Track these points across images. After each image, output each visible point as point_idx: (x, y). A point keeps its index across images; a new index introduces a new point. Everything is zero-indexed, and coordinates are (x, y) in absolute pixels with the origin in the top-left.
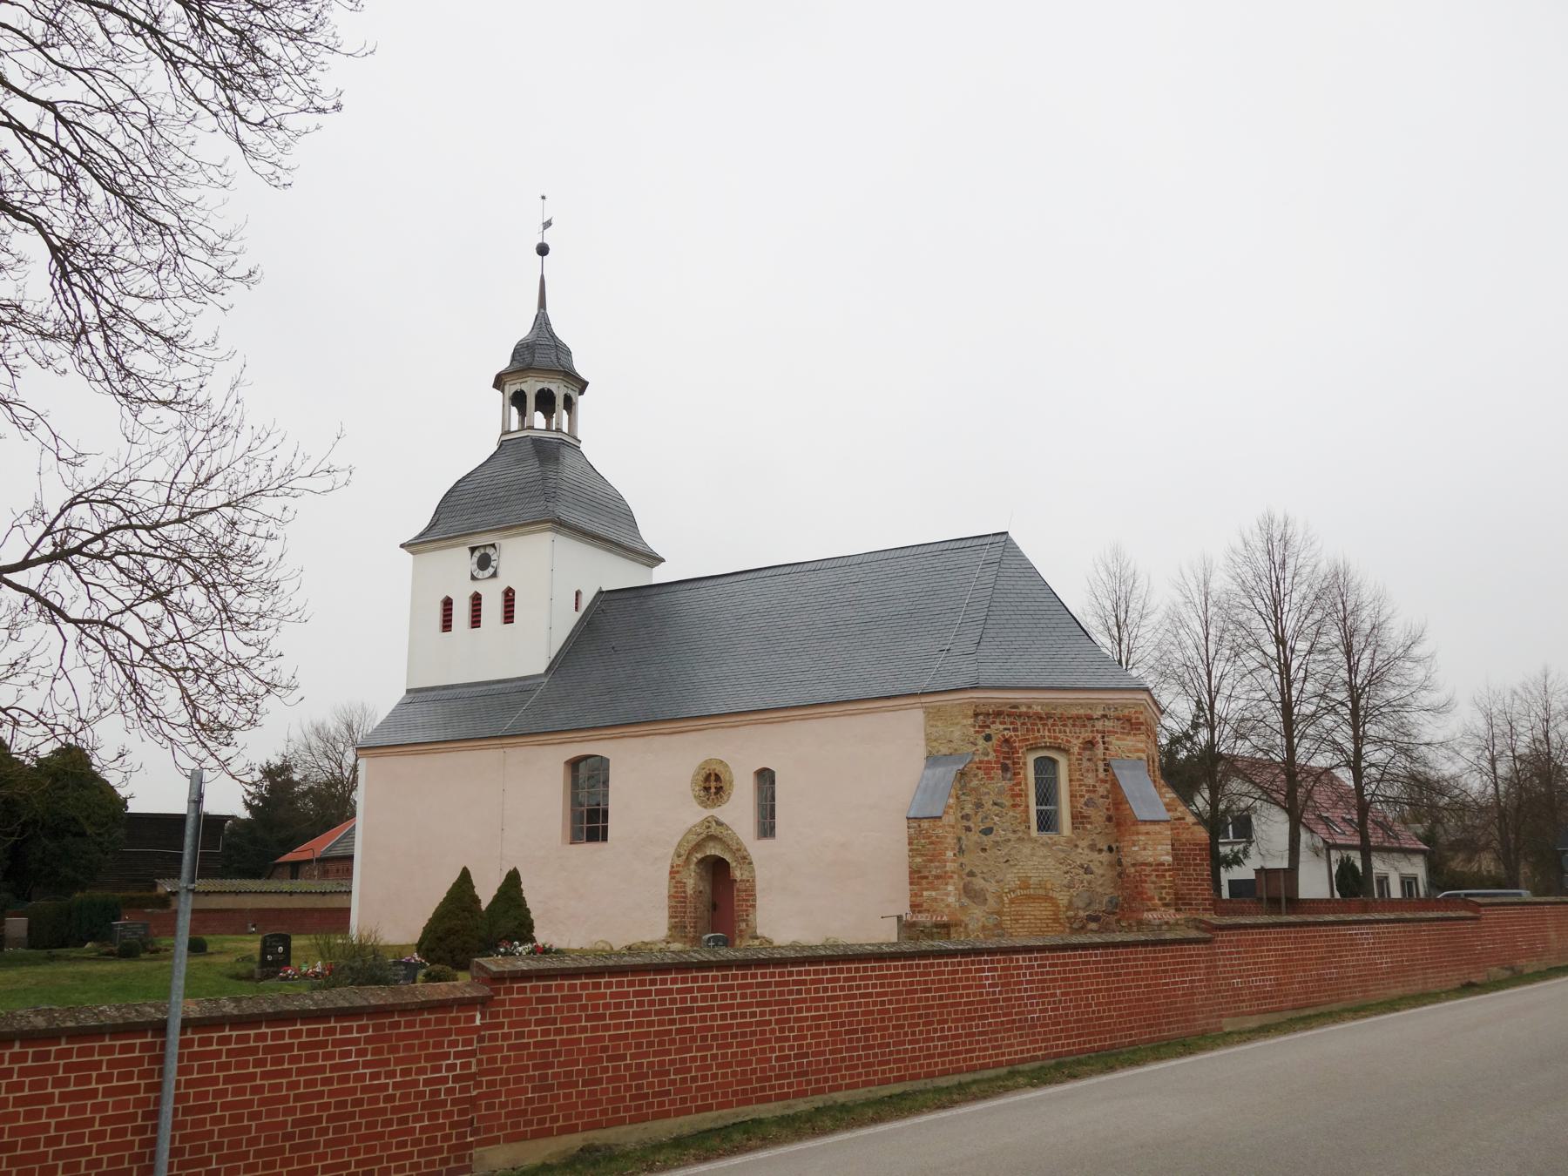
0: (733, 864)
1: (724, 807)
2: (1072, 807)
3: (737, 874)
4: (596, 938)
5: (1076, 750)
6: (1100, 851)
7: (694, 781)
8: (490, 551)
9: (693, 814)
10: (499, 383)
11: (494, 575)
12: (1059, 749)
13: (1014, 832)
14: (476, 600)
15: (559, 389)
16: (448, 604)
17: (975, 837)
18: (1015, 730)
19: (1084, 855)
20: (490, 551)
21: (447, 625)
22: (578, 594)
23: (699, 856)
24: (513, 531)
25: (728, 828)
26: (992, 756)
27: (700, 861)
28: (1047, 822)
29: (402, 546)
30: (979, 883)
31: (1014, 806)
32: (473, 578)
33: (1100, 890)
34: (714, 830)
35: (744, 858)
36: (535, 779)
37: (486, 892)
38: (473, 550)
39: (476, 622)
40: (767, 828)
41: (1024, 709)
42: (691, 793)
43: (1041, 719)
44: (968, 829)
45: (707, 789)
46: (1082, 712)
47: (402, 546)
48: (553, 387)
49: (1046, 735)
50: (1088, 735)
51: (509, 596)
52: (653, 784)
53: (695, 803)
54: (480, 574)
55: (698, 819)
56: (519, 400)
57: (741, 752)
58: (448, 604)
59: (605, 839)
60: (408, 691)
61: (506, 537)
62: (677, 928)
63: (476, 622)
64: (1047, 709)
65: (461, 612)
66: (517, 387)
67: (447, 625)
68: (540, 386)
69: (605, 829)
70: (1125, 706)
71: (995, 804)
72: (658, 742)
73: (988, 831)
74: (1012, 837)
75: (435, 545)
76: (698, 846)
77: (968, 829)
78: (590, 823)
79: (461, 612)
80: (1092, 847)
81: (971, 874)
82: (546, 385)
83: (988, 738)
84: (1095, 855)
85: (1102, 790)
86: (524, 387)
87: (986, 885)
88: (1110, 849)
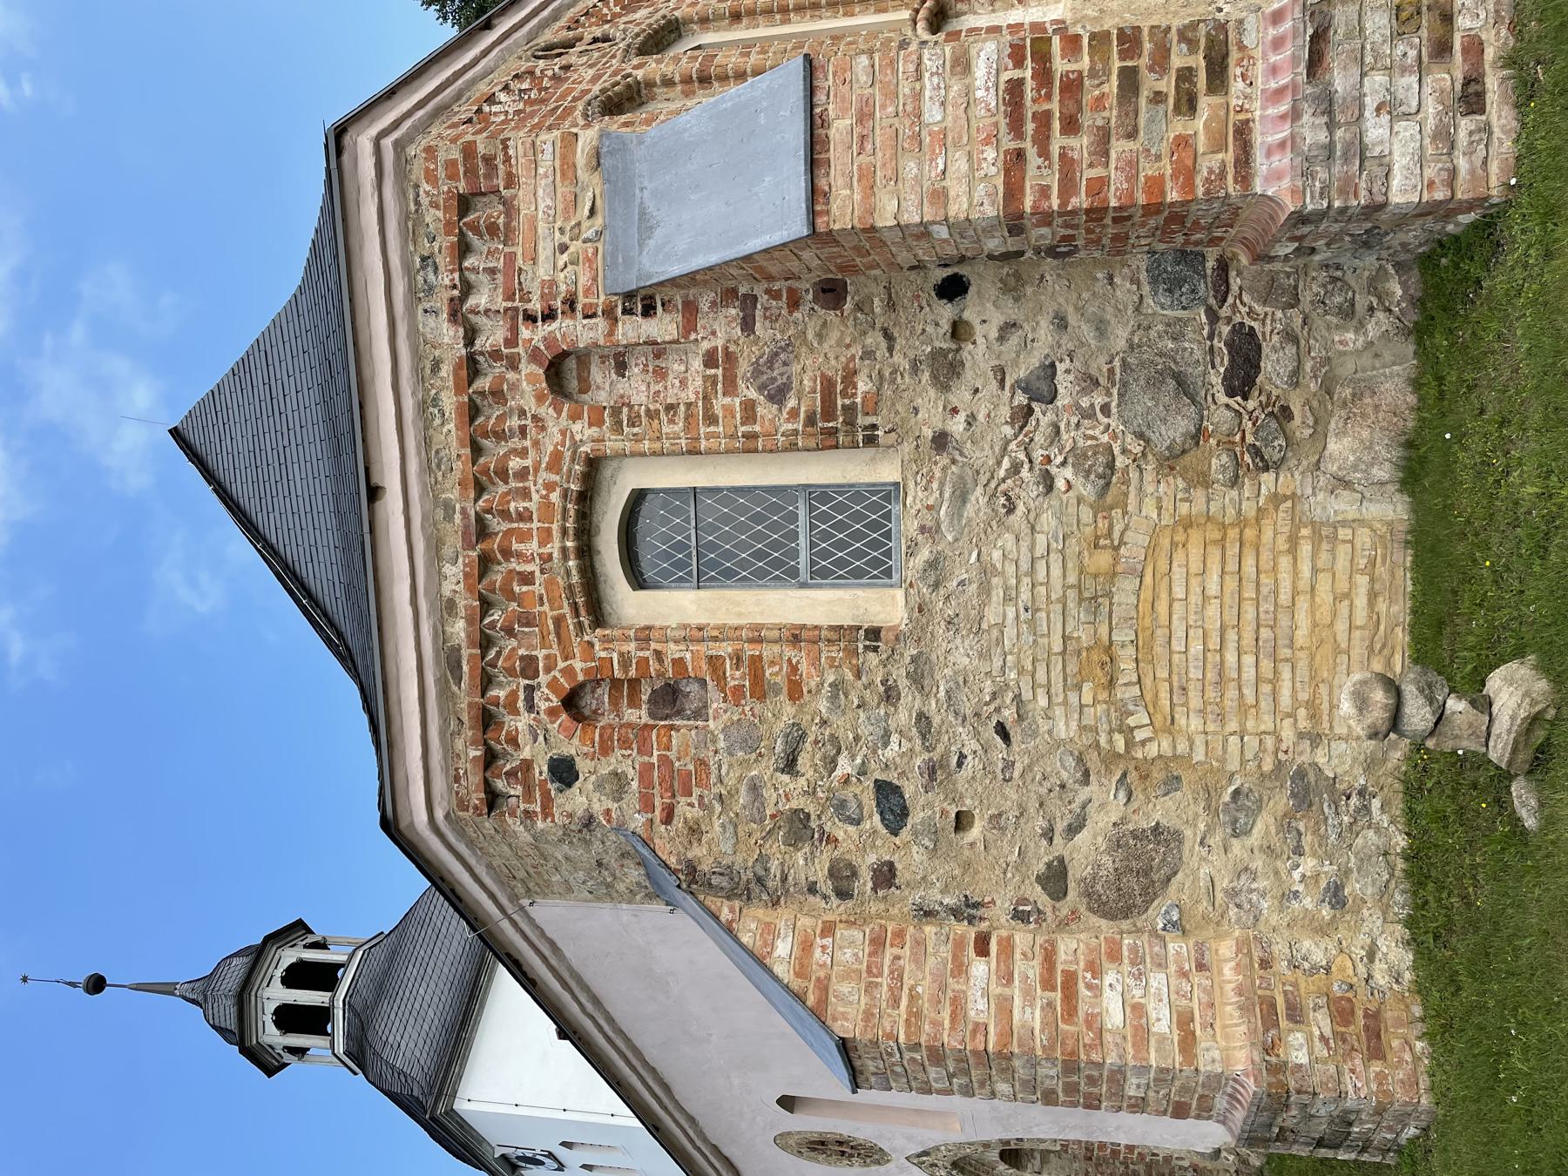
6: (959, 330)
12: (586, 499)
13: (890, 695)
15: (290, 956)
19: (980, 403)
30: (1087, 853)
31: (795, 691)
33: (1120, 337)
41: (459, 629)
44: (885, 876)
48: (271, 1007)
50: (528, 381)
61: (481, 1140)
64: (453, 542)
68: (272, 1029)
70: (412, 225)
74: (909, 701)
77: (885, 876)
80: (946, 369)
81: (1055, 879)
83: (564, 772)
84: (978, 355)
87: (1101, 822)
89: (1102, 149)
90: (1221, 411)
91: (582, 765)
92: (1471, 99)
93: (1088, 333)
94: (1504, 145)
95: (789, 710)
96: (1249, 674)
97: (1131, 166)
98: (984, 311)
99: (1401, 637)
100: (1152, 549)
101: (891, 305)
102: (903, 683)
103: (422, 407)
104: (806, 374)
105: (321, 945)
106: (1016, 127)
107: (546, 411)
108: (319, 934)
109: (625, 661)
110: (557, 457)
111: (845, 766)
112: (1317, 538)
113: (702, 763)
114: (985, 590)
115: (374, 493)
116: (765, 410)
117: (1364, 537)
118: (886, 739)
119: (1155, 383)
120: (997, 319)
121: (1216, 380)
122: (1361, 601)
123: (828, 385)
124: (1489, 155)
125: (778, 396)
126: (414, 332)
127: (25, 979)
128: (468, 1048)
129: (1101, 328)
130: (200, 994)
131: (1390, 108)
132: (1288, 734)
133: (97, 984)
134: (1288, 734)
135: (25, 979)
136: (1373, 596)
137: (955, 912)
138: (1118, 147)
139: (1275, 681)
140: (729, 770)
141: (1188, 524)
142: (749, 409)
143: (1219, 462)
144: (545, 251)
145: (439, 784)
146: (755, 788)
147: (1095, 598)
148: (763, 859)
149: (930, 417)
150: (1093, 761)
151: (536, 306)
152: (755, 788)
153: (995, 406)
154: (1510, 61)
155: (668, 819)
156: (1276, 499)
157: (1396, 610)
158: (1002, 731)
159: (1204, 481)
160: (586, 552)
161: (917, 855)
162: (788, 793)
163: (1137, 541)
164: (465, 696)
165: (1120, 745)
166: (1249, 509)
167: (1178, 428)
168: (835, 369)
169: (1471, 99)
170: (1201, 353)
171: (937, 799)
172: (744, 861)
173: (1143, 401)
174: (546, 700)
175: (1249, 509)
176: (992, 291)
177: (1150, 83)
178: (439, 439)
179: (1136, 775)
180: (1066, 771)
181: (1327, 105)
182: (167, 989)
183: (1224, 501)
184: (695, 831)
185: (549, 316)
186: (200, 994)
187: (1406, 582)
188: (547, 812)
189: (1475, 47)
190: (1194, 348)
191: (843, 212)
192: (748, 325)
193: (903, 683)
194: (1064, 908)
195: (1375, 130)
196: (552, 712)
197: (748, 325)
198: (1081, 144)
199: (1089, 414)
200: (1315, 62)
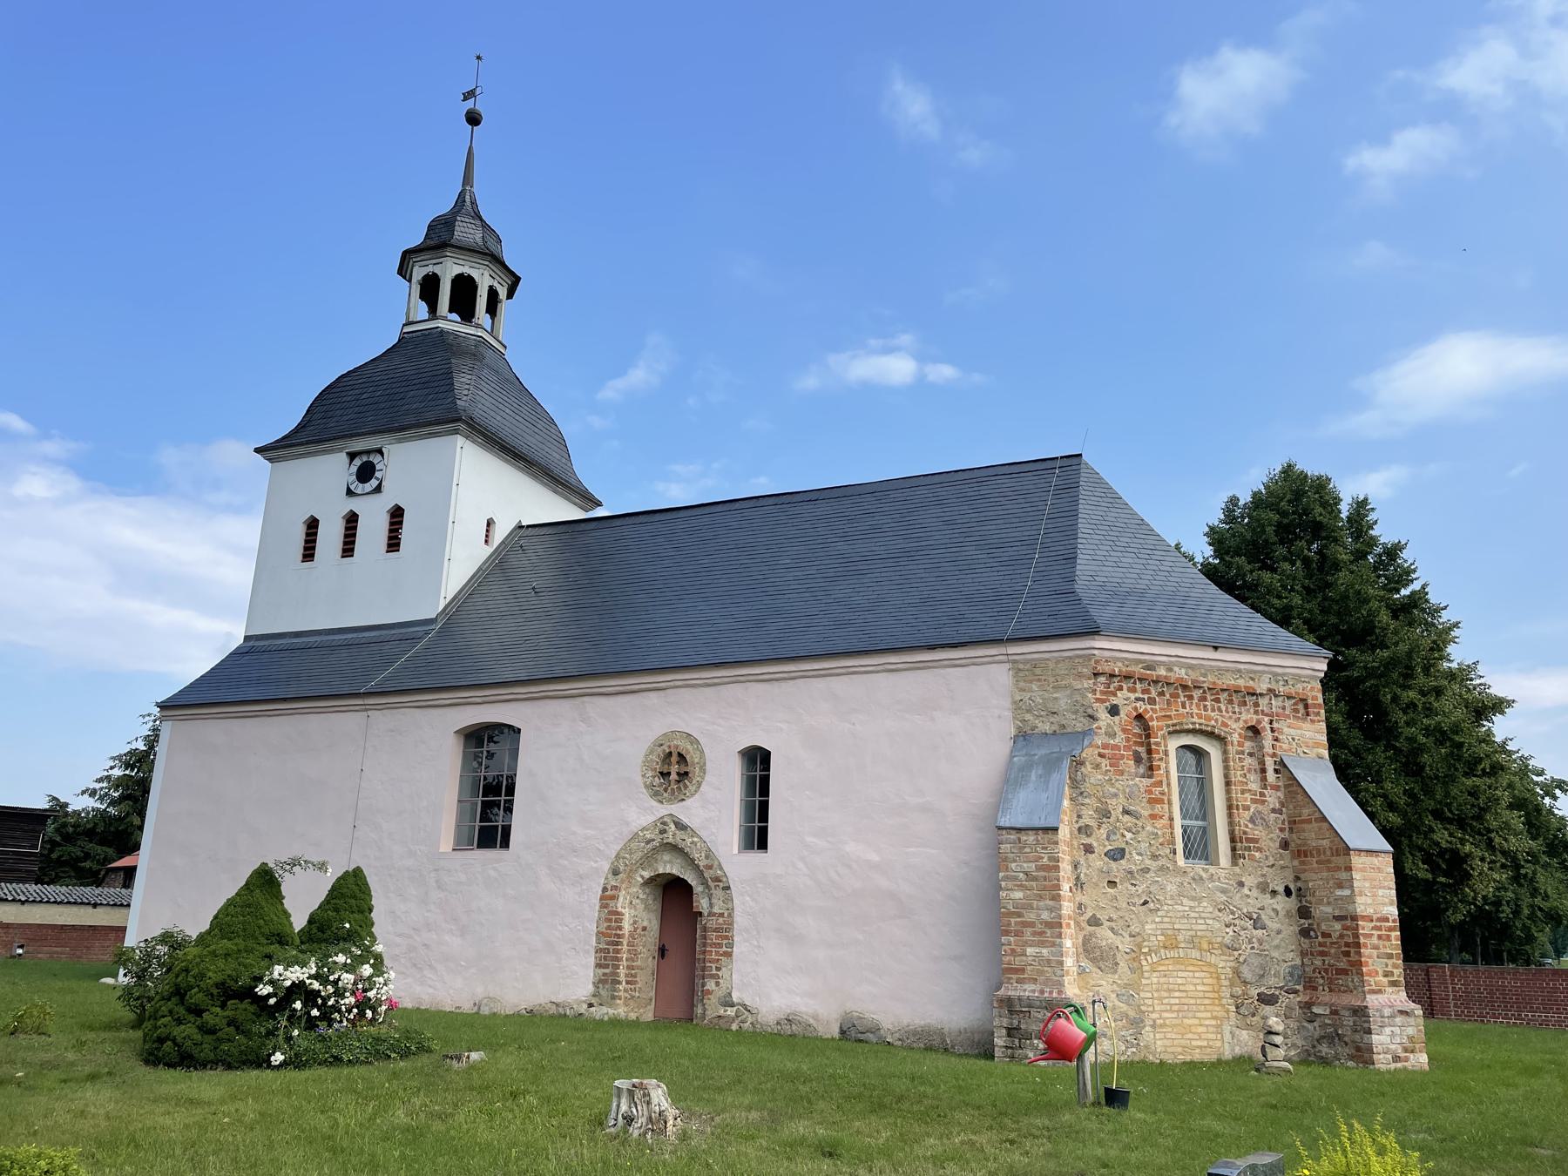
0: (698, 889)
1: (688, 802)
2: (1231, 823)
3: (702, 904)
4: (480, 991)
5: (1235, 738)
6: (1274, 893)
7: (646, 763)
8: (375, 459)
9: (643, 812)
10: (407, 259)
11: (378, 489)
12: (1210, 735)
13: (1155, 857)
14: (352, 520)
15: (484, 279)
16: (312, 525)
17: (1098, 862)
18: (1152, 701)
19: (1252, 900)
20: (375, 459)
21: (309, 554)
22: (490, 523)
23: (647, 874)
24: (407, 434)
25: (694, 833)
26: (1120, 739)
27: (649, 882)
28: (1199, 846)
29: (257, 450)
30: (1105, 935)
31: (1153, 817)
32: (350, 493)
33: (1275, 954)
34: (672, 834)
35: (718, 880)
36: (416, 755)
37: (301, 900)
38: (352, 456)
39: (348, 549)
40: (757, 838)
41: (1162, 672)
42: (639, 780)
43: (1185, 687)
44: (1089, 849)
45: (665, 775)
46: (1241, 682)
47: (257, 450)
48: (475, 274)
49: (1194, 713)
50: (1249, 716)
51: (397, 514)
52: (588, 762)
53: (645, 795)
54: (359, 488)
55: (647, 820)
56: (429, 288)
57: (720, 716)
58: (312, 525)
59: (505, 844)
60: (247, 638)
61: (400, 441)
62: (606, 983)
63: (348, 549)
64: (1194, 675)
65: (330, 536)
66: (430, 269)
67: (309, 554)
68: (457, 270)
69: (507, 831)
70: (1298, 678)
71: (1126, 812)
72: (595, 706)
73: (1117, 855)
74: (1152, 865)
75: (302, 449)
76: (648, 859)
77: (1089, 849)
78: (489, 816)
79: (330, 536)
80: (1263, 887)
81: (1094, 922)
82: (467, 270)
83: (1114, 711)
84: (1267, 900)
85: (1273, 799)
86: (437, 270)
87: (1117, 941)
88: (1288, 892)
89: (1376, 947)
90: (1254, 992)
91: (1117, 718)
92: (1396, 1059)
93: (1276, 942)
94: (1383, 1067)
95: (1146, 813)
96: (1173, 1001)
97: (1370, 957)
98: (1281, 903)
99: (1188, 1058)
100: (1210, 964)
101: (1283, 867)
102: (1160, 863)
103: (1239, 671)
104: (1258, 832)
105: (492, 308)
106: (1379, 920)
107: (1241, 724)
108: (505, 306)
109: (1157, 744)
110: (1226, 725)
111: (1129, 835)
112: (1217, 1026)
113: (1122, 773)
114: (1193, 899)
115: (1216, 648)
116: (1247, 815)
117: (1219, 1044)
118: (1140, 854)
119: (1263, 967)
120: (1279, 908)
121: (1263, 989)
122: (1199, 1043)
123: (1256, 841)
124: (1382, 1062)
125: (1252, 820)
126: (1264, 672)
127: (479, 58)
128: (489, 450)
129: (1277, 947)
130: (465, 205)
131: (1393, 1034)
132: (1154, 1016)
133: (473, 119)
134: (1154, 1016)
135: (479, 58)
136: (1200, 1047)
137: (1078, 878)
138: (1375, 952)
139: (1171, 1011)
140: (1122, 783)
141: (1218, 978)
142: (1247, 808)
143: (1238, 991)
144: (1292, 732)
145: (1107, 654)
146: (1116, 795)
147: (1193, 942)
148: (1089, 796)
149: (1250, 881)
150: (1139, 939)
151: (1275, 725)
152: (1116, 795)
153: (1251, 906)
154: (1405, 1068)
155: (1101, 755)
156: (1228, 1011)
157: (1197, 1056)
158: (1145, 903)
159: (1232, 985)
160: (1188, 731)
161: (1099, 864)
162: (1116, 806)
163: (1213, 959)
164: (1138, 670)
165: (1145, 950)
166: (1224, 1001)
167: (1247, 973)
168: (1261, 844)
169: (1396, 1059)
170: (1273, 982)
171: (1122, 874)
172: (1086, 787)
173: (1255, 961)
174: (1141, 707)
175: (1224, 1001)
176: (1288, 906)
177: (1390, 962)
178: (1229, 675)
179: (1136, 955)
180: (1135, 928)
181: (1392, 1016)
182: (468, 178)
183: (1226, 992)
184: (1097, 766)
185: (1273, 730)
186: (465, 205)
187: (1206, 1059)
188: (1098, 700)
189: (1407, 1059)
190: (1272, 981)
191: (1357, 861)
192: (1274, 811)
193: (1160, 863)
194: (1084, 925)
195: (1388, 1030)
196: (1136, 709)
197: (1274, 811)
198: (1375, 940)
199: (1250, 942)
200: (1401, 1012)
